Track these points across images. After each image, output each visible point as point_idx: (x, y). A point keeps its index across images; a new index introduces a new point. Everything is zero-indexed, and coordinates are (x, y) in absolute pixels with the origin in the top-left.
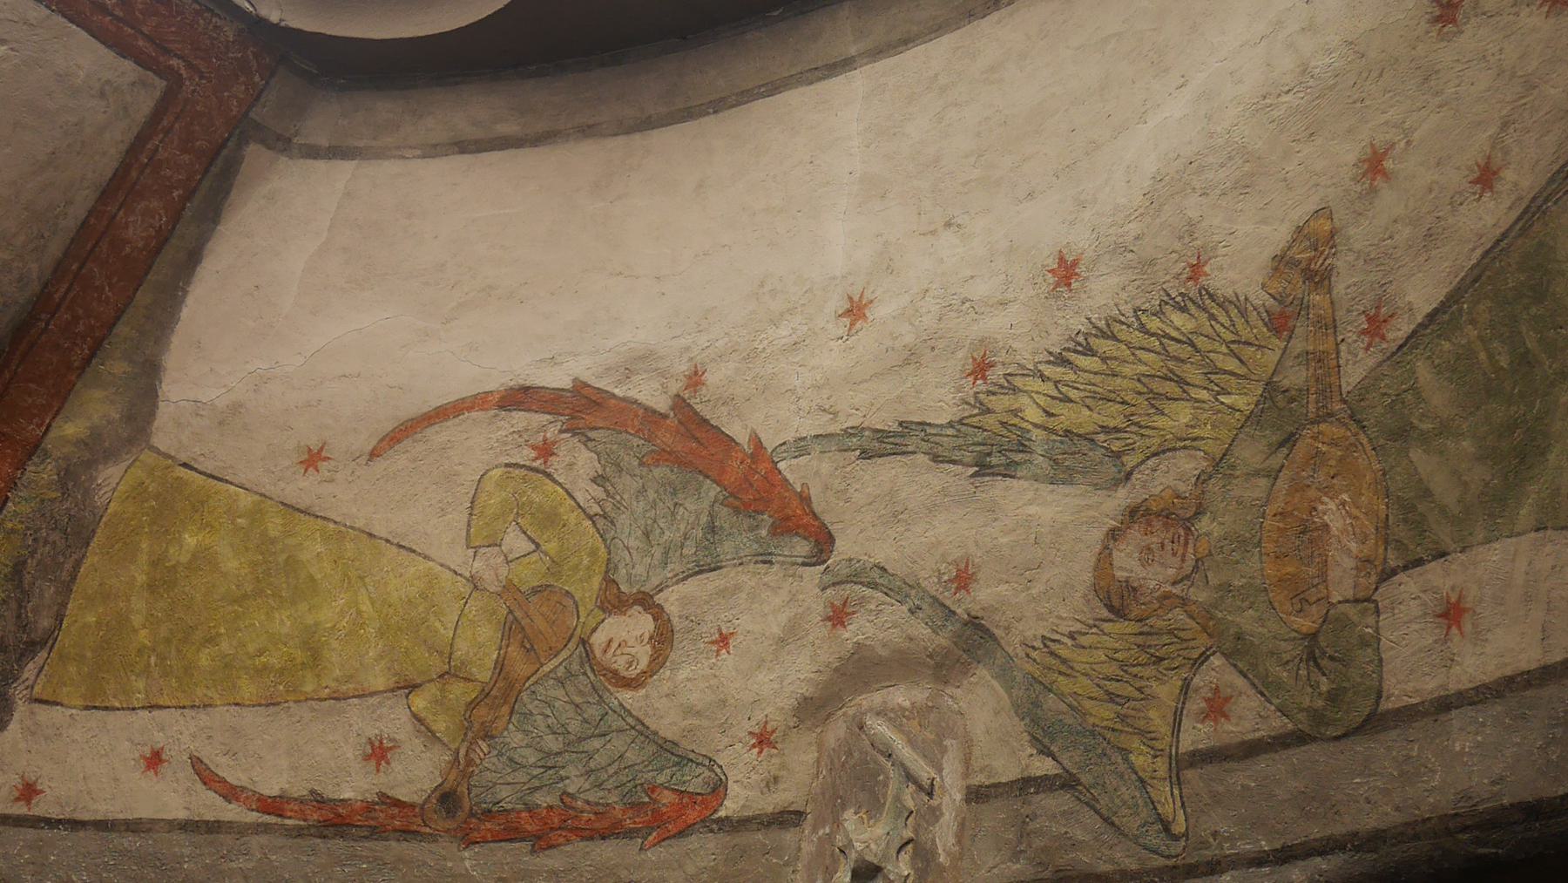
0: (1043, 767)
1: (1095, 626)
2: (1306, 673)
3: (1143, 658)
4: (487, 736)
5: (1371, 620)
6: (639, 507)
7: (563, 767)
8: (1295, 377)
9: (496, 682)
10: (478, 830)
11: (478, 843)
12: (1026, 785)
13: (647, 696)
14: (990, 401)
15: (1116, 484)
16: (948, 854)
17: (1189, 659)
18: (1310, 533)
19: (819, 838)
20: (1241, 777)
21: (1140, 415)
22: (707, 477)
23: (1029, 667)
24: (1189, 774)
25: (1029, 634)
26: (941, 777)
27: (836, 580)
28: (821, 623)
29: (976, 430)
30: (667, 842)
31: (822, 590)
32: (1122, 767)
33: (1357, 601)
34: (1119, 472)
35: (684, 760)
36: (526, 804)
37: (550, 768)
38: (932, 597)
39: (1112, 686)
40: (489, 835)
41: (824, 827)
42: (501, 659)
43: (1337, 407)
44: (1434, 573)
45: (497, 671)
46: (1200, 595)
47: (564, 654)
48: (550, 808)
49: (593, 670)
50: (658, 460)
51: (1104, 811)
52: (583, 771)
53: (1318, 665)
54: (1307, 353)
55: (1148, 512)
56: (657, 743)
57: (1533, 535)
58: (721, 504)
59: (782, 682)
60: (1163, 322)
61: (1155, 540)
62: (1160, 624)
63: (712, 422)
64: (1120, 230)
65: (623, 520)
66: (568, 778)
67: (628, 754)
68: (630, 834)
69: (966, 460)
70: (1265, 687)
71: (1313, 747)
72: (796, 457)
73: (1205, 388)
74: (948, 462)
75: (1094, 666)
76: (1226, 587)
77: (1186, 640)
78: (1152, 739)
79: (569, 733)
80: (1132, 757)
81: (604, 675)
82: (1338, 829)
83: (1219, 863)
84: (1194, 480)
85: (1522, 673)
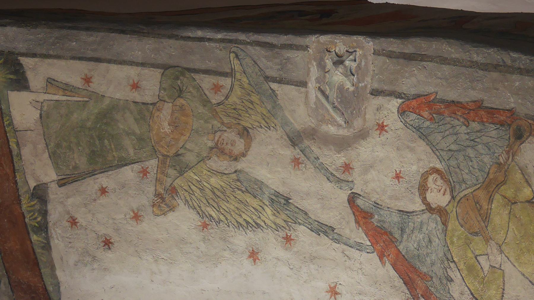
0: (274, 86)
1: (254, 128)
2: (184, 87)
3: (240, 112)
4: (500, 164)
5: (161, 94)
6: (433, 257)
7: (467, 139)
8: (171, 172)
9: (493, 191)
10: (507, 117)
11: (507, 110)
12: (280, 81)
13: (429, 162)
14: (284, 225)
15: (240, 171)
16: (313, 65)
17: (224, 106)
18: (174, 124)
19: (364, 82)
20: (211, 65)
21: (229, 190)
22: (403, 256)
23: (276, 121)
24: (228, 71)
25: (274, 133)
26: (316, 94)
27: (348, 183)
28: (354, 168)
29: (289, 216)
30: (426, 93)
31: (353, 181)
32: (250, 79)
33: (164, 101)
34: (238, 174)
35: (418, 129)
36: (484, 125)
37: (472, 140)
38: (309, 160)
39: (251, 106)
40: (502, 113)
41: (362, 86)
42: (490, 203)
43: (160, 157)
44: (138, 99)
45: (492, 197)
46: (216, 123)
47: (462, 195)
48: (474, 121)
49: (450, 182)
50: (424, 275)
51: (257, 66)
52: (459, 135)
53: (180, 88)
54: (167, 176)
55: (231, 157)
56: (428, 140)
57: (106, 95)
58: (398, 240)
59: (373, 150)
60: (219, 216)
61: (229, 147)
62: (233, 120)
63: (402, 282)
64: (232, 257)
65: (441, 255)
66: (465, 133)
67: (441, 138)
68: (442, 101)
69: (293, 206)
70: (199, 88)
71: (185, 66)
72: (362, 243)
73: (205, 186)
74: (301, 209)
75: (255, 114)
76: (206, 122)
77: (224, 112)
78: (240, 85)
79: (463, 155)
80: (247, 81)
81: (446, 178)
82: (182, 42)
83: (221, 42)
84: (212, 159)
85: (116, 64)
